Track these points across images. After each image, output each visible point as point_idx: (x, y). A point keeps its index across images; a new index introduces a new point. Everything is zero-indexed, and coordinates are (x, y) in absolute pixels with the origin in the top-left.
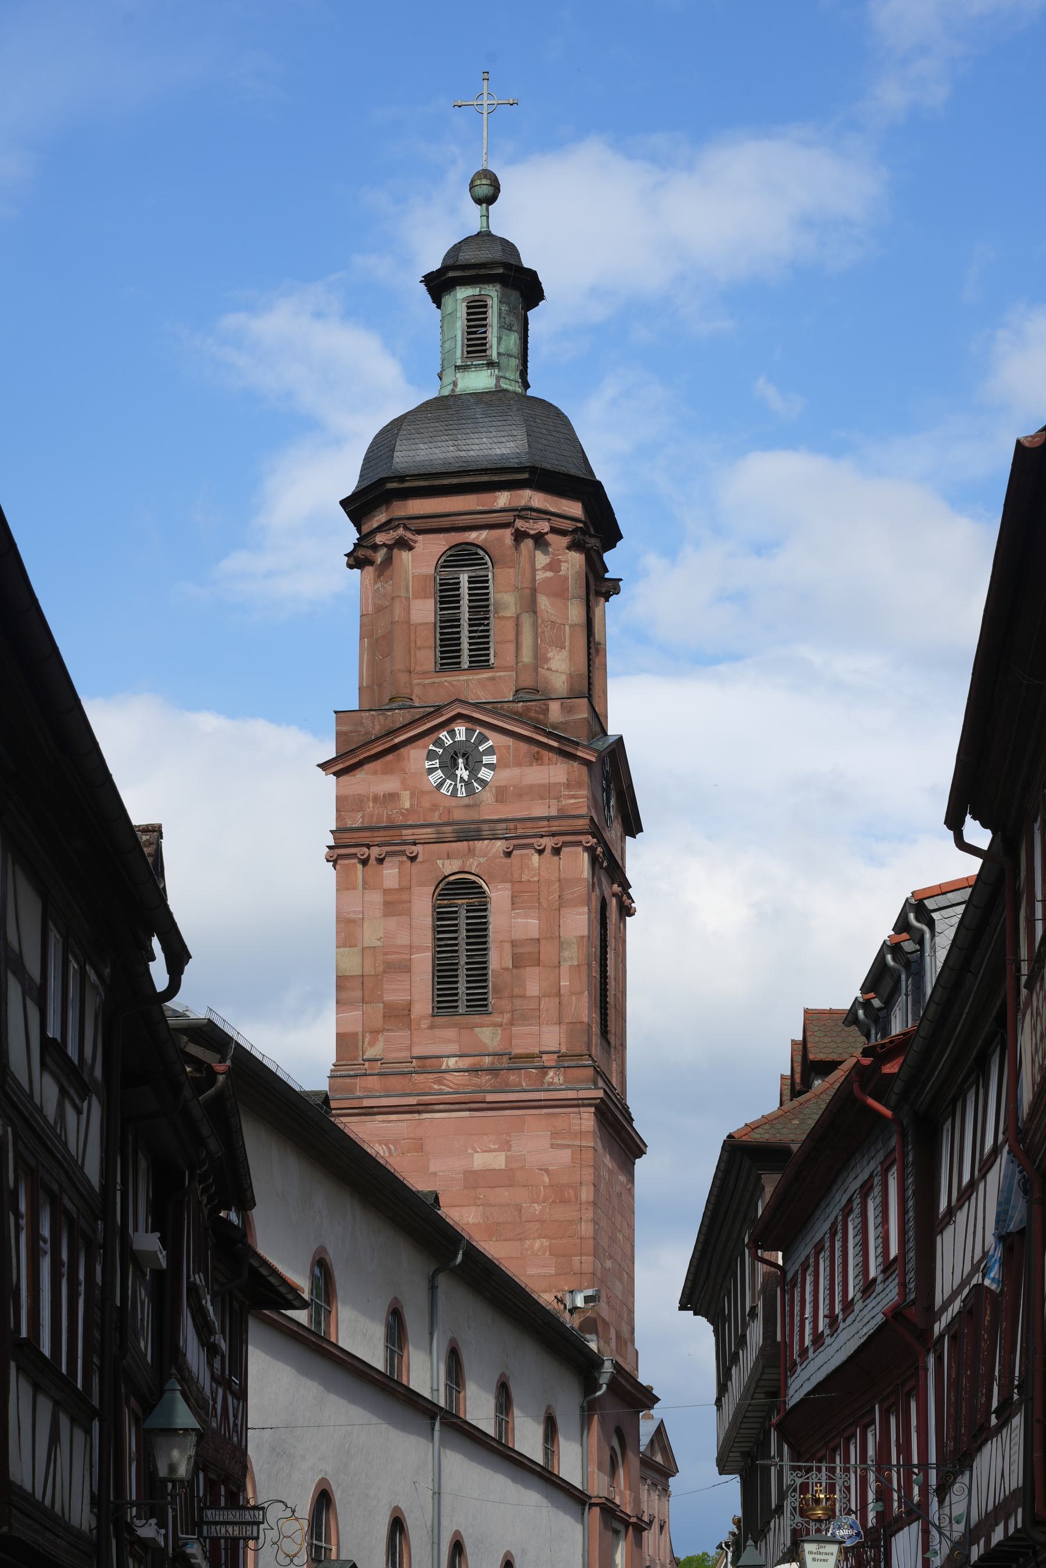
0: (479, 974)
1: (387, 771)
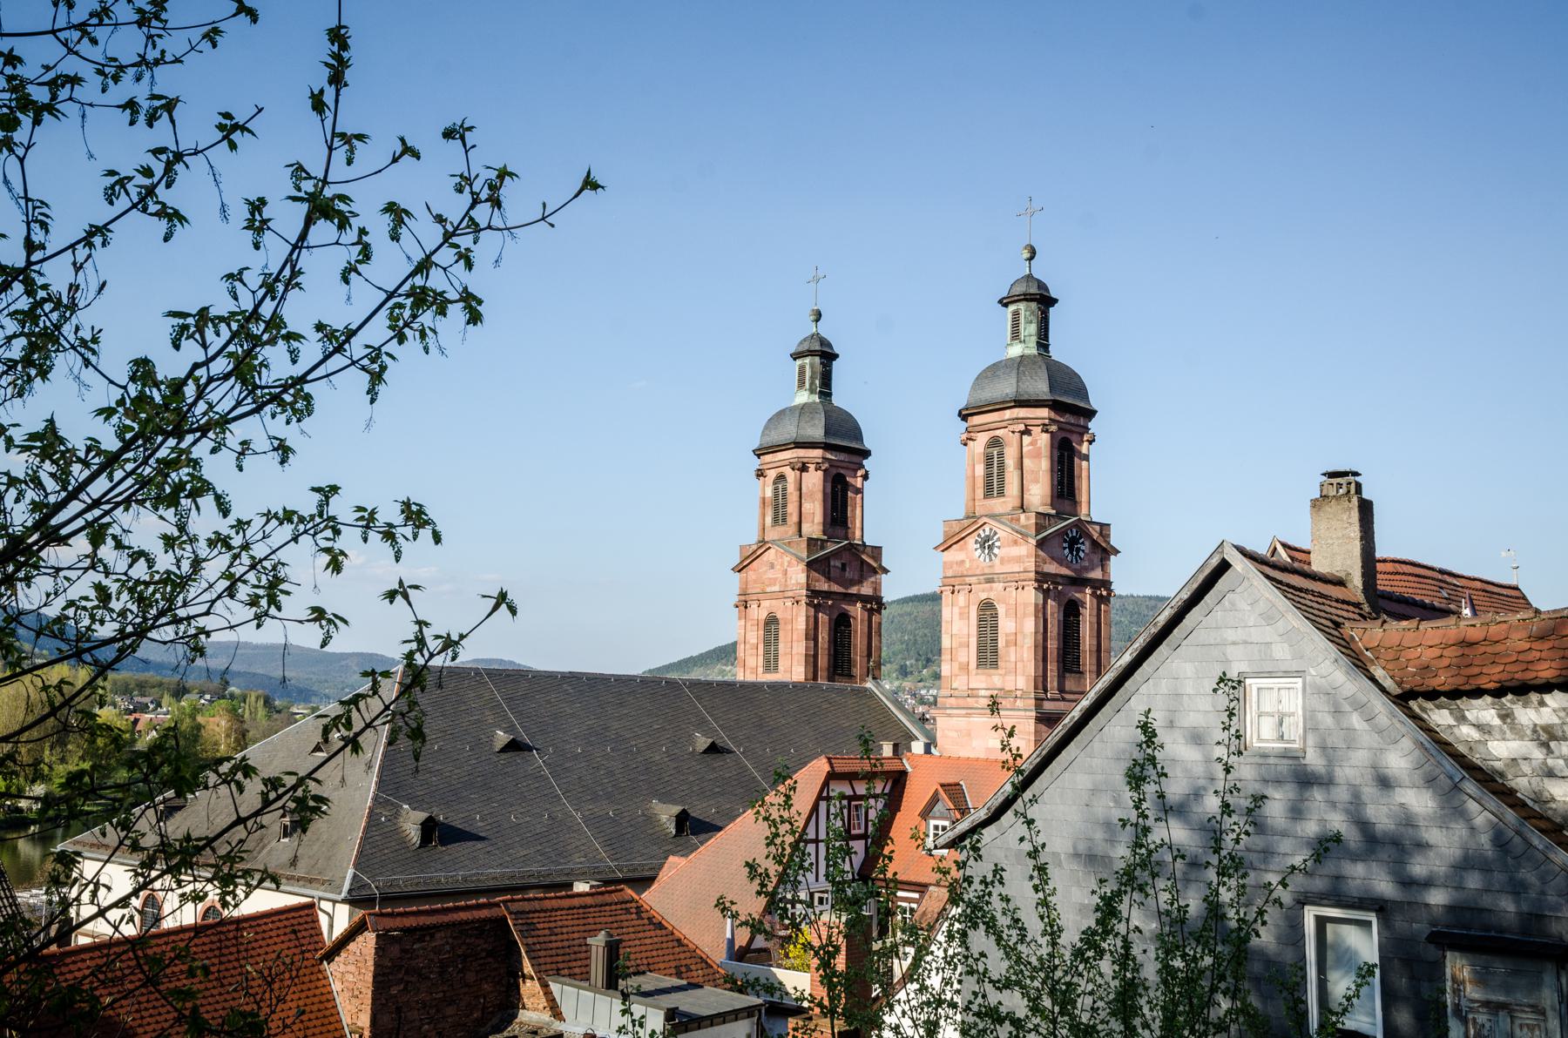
0: (995, 652)
1: (961, 549)
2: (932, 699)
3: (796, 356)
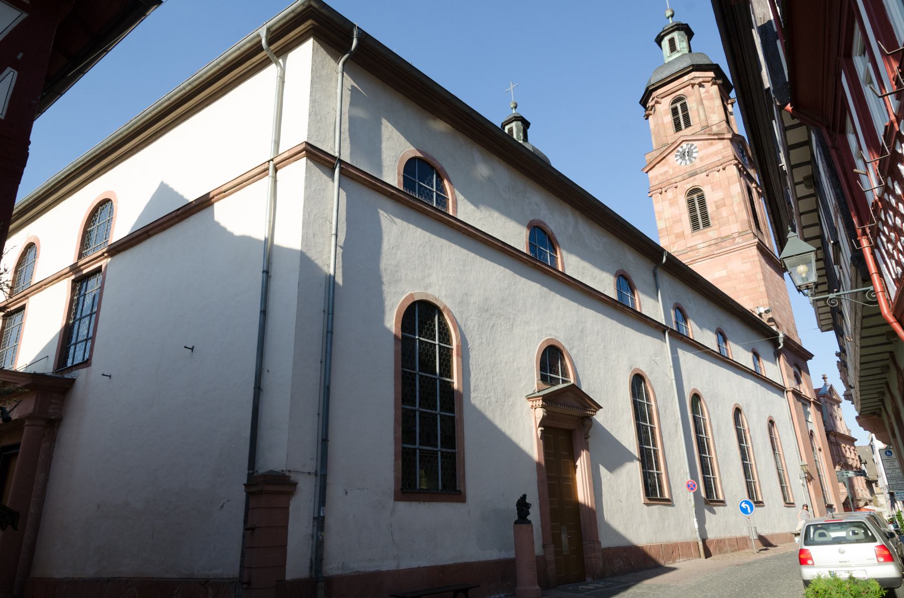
1: (663, 165)
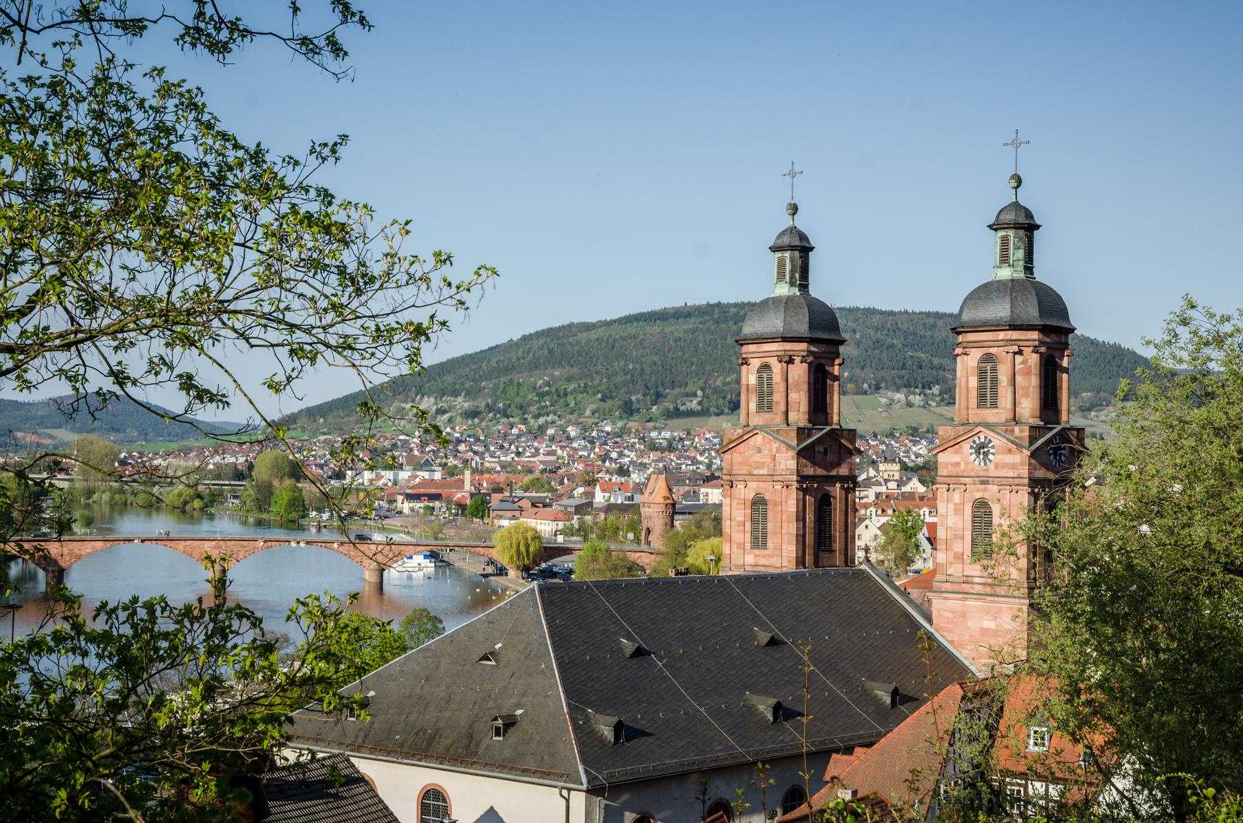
1: (956, 452)
2: (665, 443)
3: (774, 249)
